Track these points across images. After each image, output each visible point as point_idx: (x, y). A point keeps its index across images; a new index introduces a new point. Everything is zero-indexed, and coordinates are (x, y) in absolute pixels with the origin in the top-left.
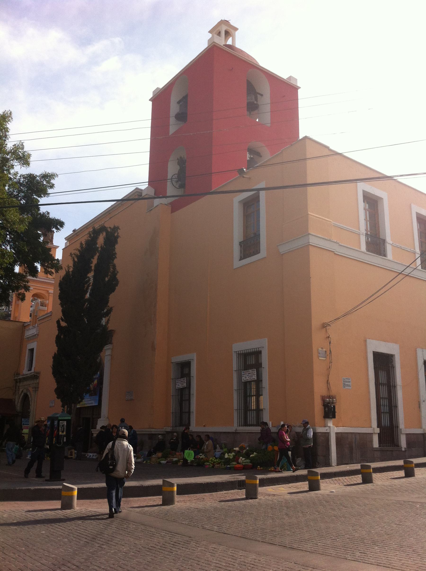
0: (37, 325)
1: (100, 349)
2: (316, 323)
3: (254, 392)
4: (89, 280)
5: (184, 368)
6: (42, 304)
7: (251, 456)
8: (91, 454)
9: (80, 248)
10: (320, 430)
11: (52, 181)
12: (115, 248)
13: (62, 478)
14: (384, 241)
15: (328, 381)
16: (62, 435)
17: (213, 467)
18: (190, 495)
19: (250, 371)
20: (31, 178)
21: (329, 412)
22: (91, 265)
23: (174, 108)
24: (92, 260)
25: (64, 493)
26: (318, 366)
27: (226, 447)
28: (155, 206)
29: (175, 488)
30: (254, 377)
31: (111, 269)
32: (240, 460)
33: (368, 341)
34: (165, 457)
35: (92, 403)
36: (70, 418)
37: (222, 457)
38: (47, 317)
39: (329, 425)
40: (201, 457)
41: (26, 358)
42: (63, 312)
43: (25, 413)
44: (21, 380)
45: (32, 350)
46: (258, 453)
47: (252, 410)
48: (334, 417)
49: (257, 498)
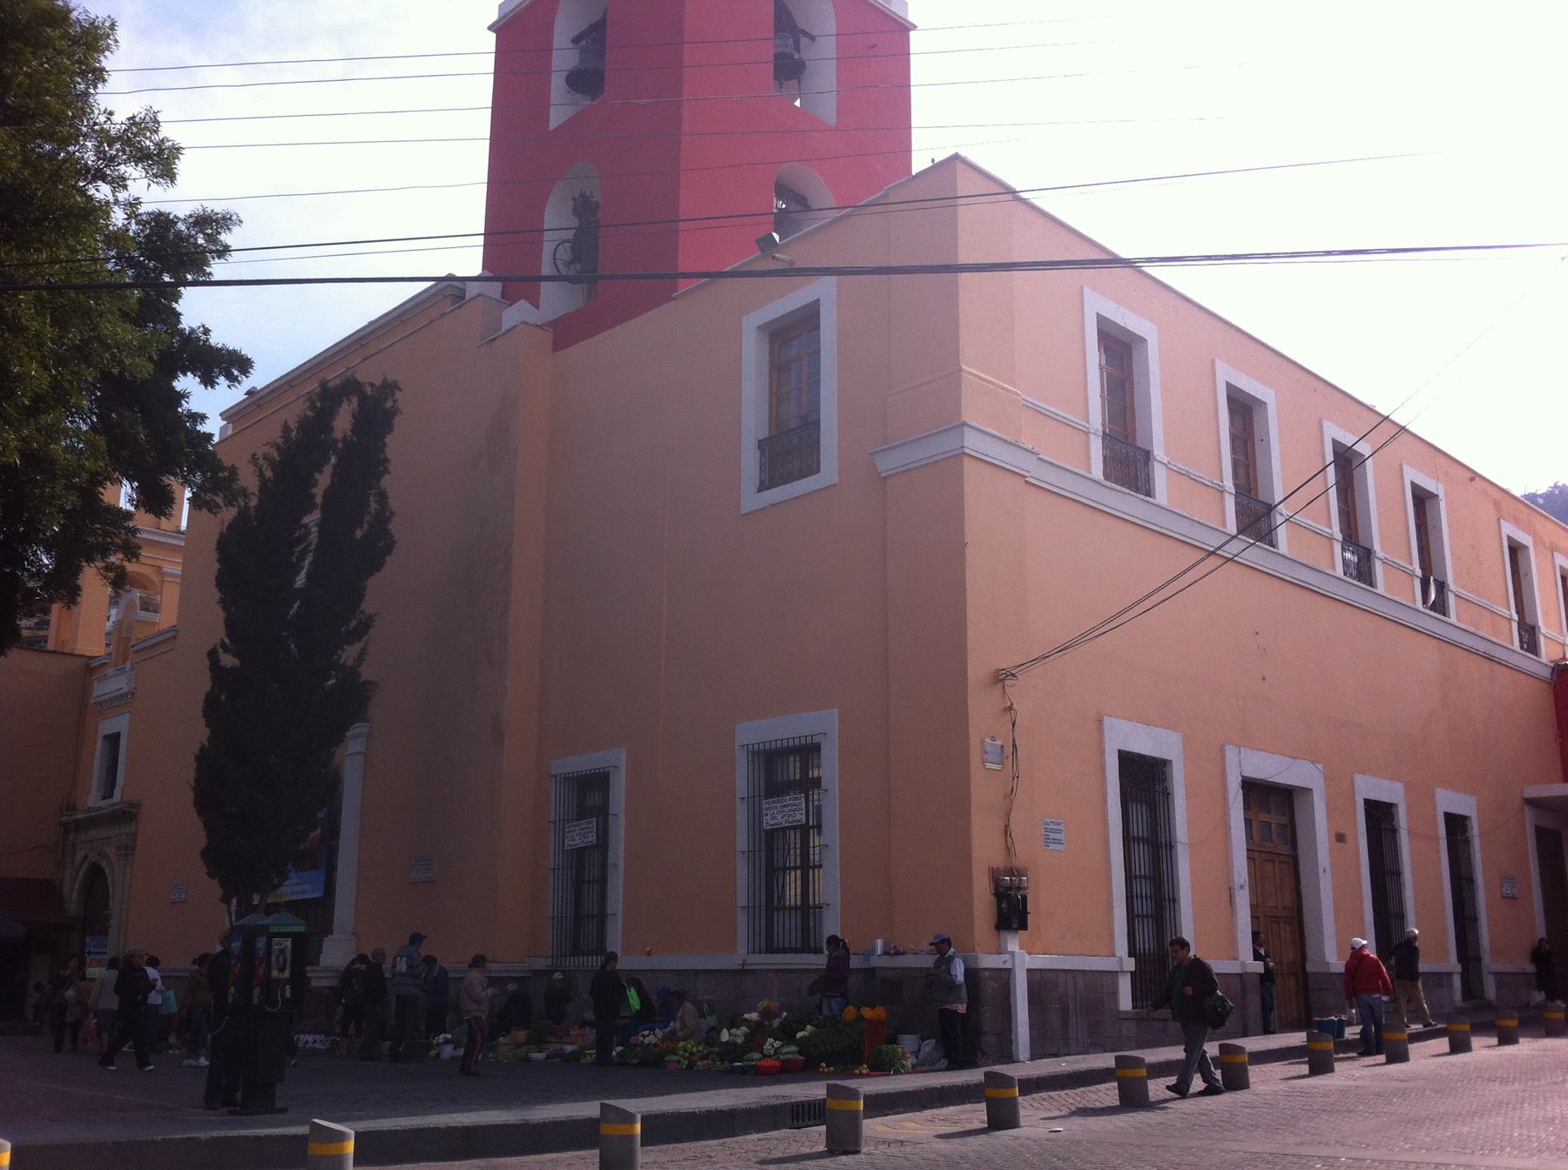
0: (128, 665)
1: (335, 736)
2: (977, 669)
3: (794, 859)
4: (308, 534)
5: (589, 792)
6: (147, 606)
7: (799, 1035)
8: (310, 1038)
9: (279, 441)
10: (989, 961)
11: (225, 237)
12: (384, 444)
13: (279, 1104)
14: (1147, 455)
15: (1007, 827)
16: (278, 980)
17: (691, 1066)
18: (665, 1147)
19: (787, 800)
20: (161, 223)
21: (1012, 912)
22: (314, 491)
23: (564, 58)
24: (317, 476)
25: (315, 1149)
26: (984, 787)
27: (712, 1013)
28: (504, 328)
29: (638, 1127)
30: (798, 817)
31: (373, 505)
32: (767, 1047)
33: (1107, 721)
34: (538, 1042)
35: (305, 891)
36: (302, 929)
37: (711, 1037)
38: (162, 642)
39: (1010, 948)
40: (647, 1040)
41: (98, 754)
42: (230, 625)
43: (94, 920)
44: (80, 826)
45: (113, 740)
46: (816, 1026)
47: (784, 908)
48: (1023, 926)
49: (857, 1152)
